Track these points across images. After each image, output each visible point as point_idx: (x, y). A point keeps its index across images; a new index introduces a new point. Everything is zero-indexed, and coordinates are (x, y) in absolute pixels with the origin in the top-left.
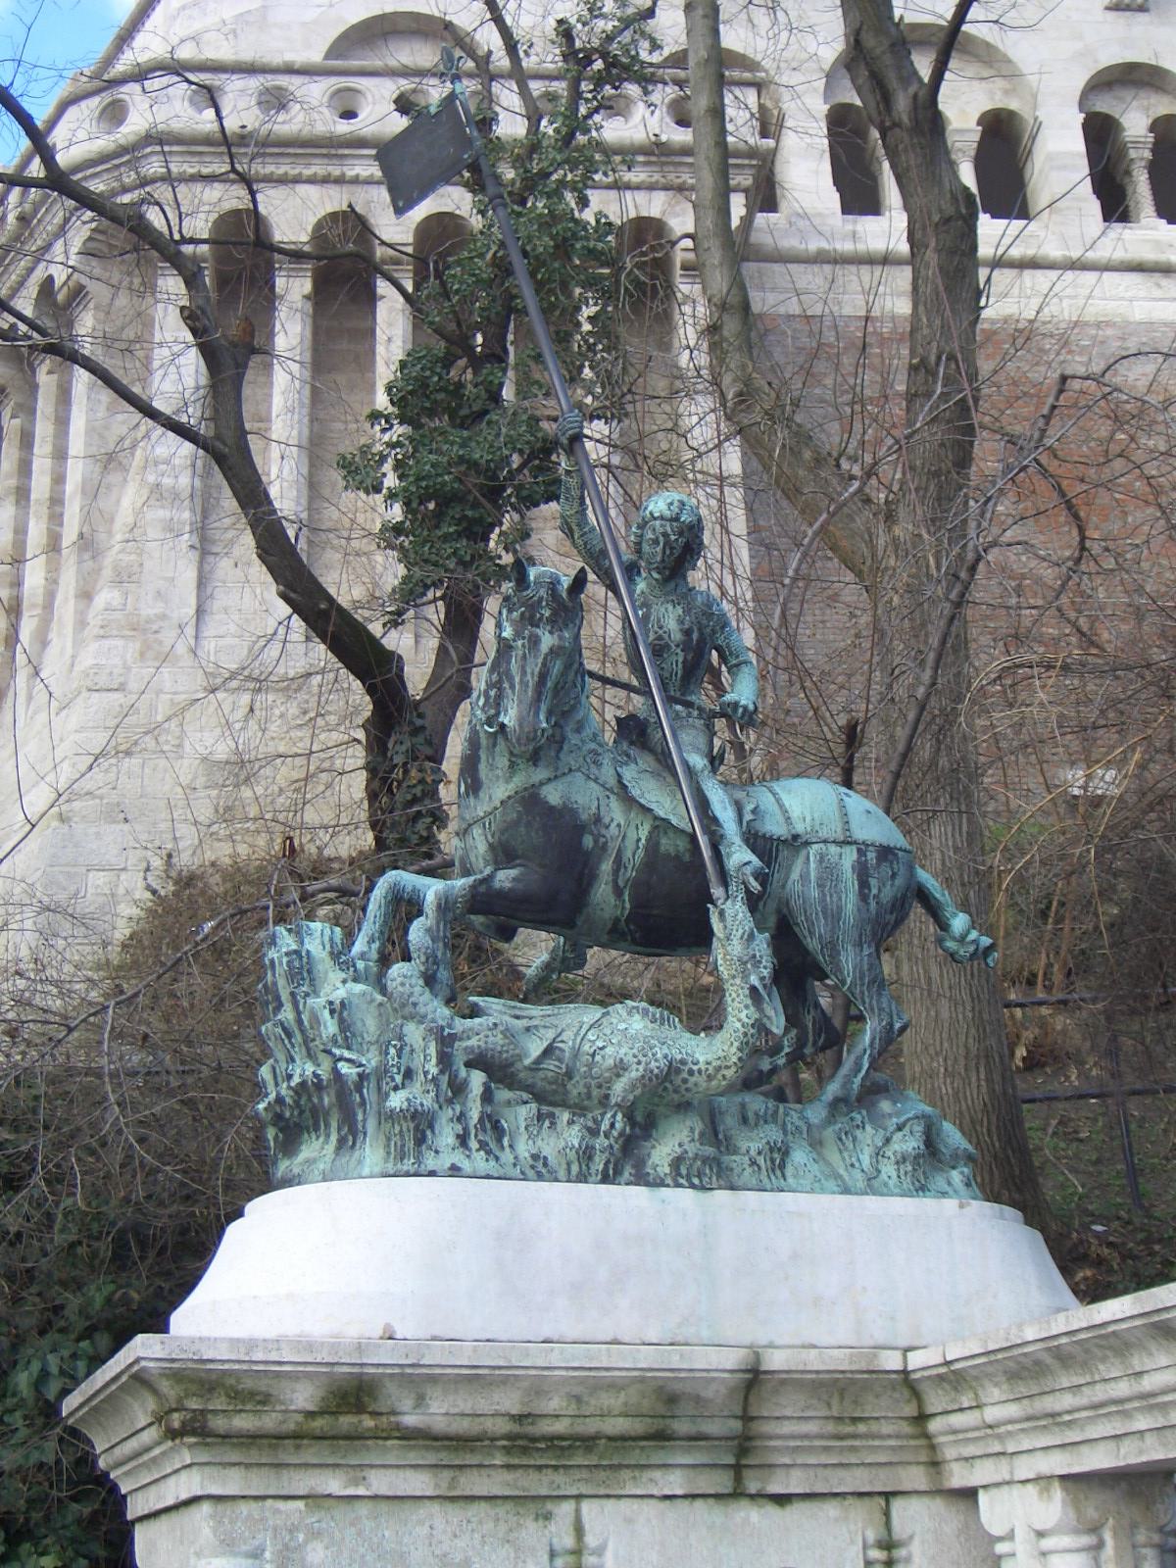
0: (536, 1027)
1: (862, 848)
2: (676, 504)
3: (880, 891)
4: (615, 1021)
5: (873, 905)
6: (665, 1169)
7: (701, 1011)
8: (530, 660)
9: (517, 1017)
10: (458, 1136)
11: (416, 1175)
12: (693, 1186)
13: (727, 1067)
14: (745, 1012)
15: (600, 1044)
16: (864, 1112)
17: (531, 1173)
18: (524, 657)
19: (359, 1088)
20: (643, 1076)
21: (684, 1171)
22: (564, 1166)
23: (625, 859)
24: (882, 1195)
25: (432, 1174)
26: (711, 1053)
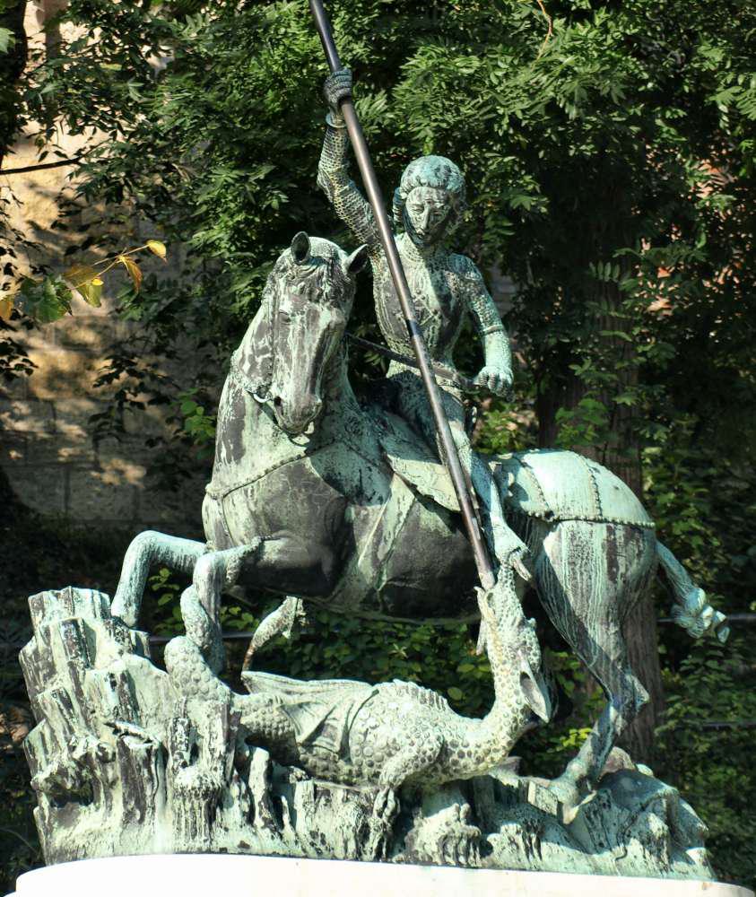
0: (308, 704)
1: (611, 527)
2: (443, 170)
3: (627, 570)
4: (385, 700)
5: (620, 581)
6: (432, 847)
7: (474, 697)
8: (308, 335)
9: (289, 693)
10: (244, 814)
11: (209, 851)
12: (459, 865)
13: (496, 751)
14: (515, 697)
15: (372, 723)
16: (609, 791)
17: (311, 851)
18: (302, 332)
19: (147, 762)
20: (416, 758)
21: (451, 850)
22: (342, 844)
23: (385, 533)
24: (630, 875)
25: (223, 851)
26: (484, 740)
